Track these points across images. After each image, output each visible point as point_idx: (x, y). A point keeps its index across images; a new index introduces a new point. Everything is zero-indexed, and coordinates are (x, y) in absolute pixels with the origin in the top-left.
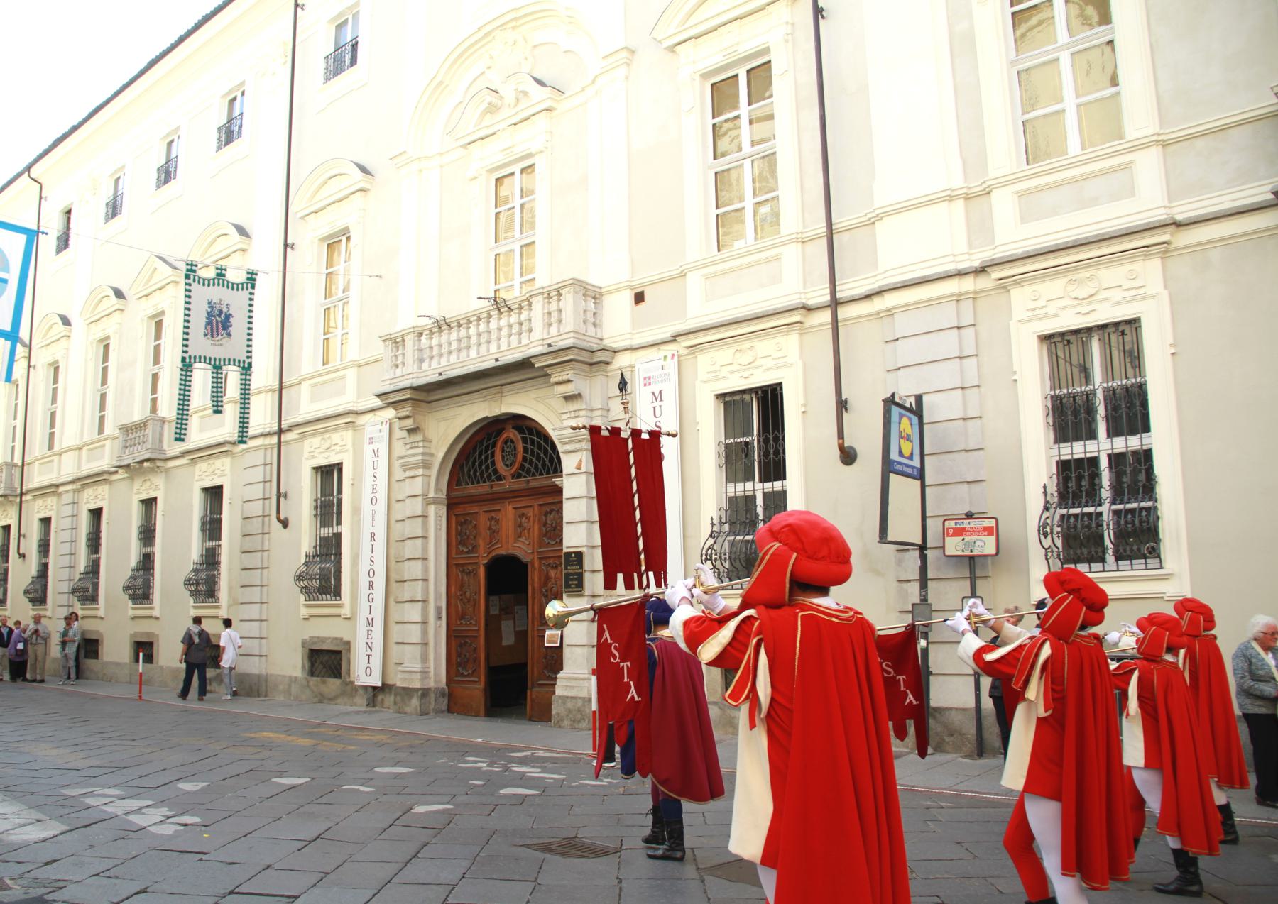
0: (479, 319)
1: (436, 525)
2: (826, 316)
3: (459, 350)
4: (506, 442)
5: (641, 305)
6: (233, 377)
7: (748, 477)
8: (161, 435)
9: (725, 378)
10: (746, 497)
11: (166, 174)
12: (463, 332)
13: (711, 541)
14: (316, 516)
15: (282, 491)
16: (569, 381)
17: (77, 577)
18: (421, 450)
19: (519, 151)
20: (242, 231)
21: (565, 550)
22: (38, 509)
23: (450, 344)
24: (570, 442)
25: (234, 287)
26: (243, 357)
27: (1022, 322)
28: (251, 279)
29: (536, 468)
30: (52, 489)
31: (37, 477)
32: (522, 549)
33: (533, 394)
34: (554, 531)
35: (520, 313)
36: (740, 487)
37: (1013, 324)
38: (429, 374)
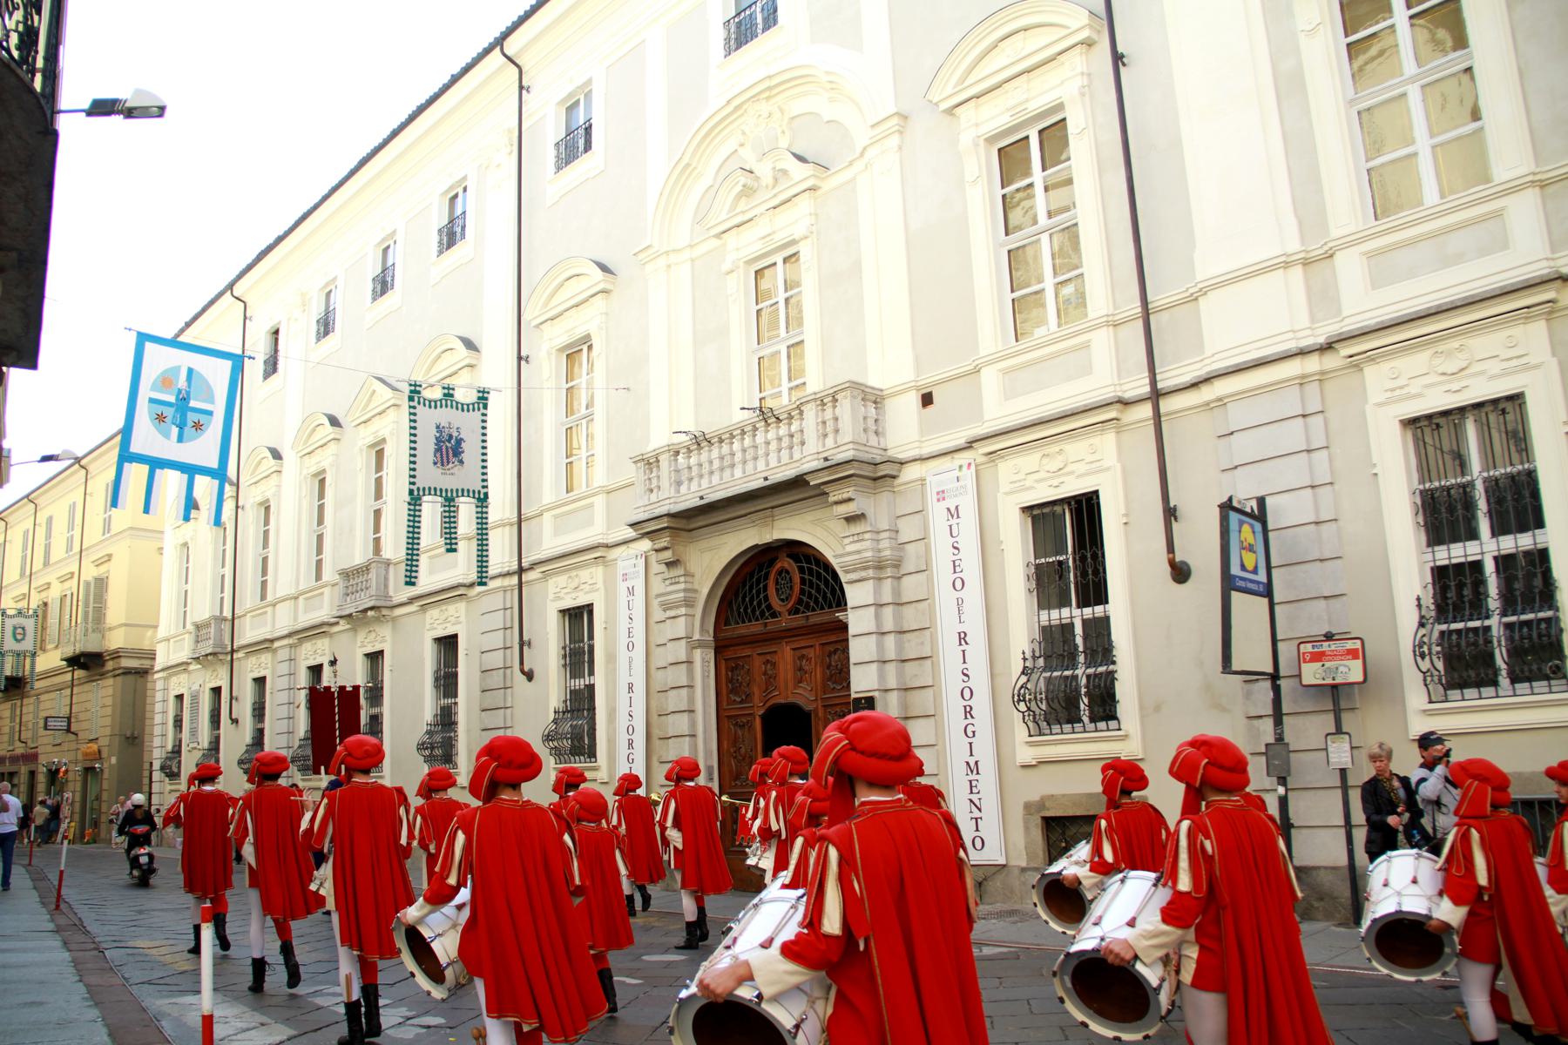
0: (743, 433)
1: (703, 671)
2: (1146, 410)
3: (722, 469)
4: (780, 573)
5: (930, 408)
6: (466, 511)
7: (1064, 602)
8: (386, 579)
9: (1419, 395)
10: (1062, 626)
11: (383, 285)
12: (725, 448)
13: (1024, 679)
14: (565, 666)
15: (525, 638)
16: (850, 500)
17: (297, 744)
18: (682, 586)
19: (780, 237)
20: (469, 345)
21: (854, 696)
22: (250, 668)
23: (711, 462)
24: (854, 571)
25: (465, 408)
26: (478, 486)
27: (1379, 405)
28: (483, 398)
29: (816, 602)
30: (265, 645)
31: (249, 633)
32: (804, 696)
33: (809, 517)
34: (840, 673)
35: (790, 424)
36: (1055, 614)
37: (1369, 409)
38: (689, 498)
